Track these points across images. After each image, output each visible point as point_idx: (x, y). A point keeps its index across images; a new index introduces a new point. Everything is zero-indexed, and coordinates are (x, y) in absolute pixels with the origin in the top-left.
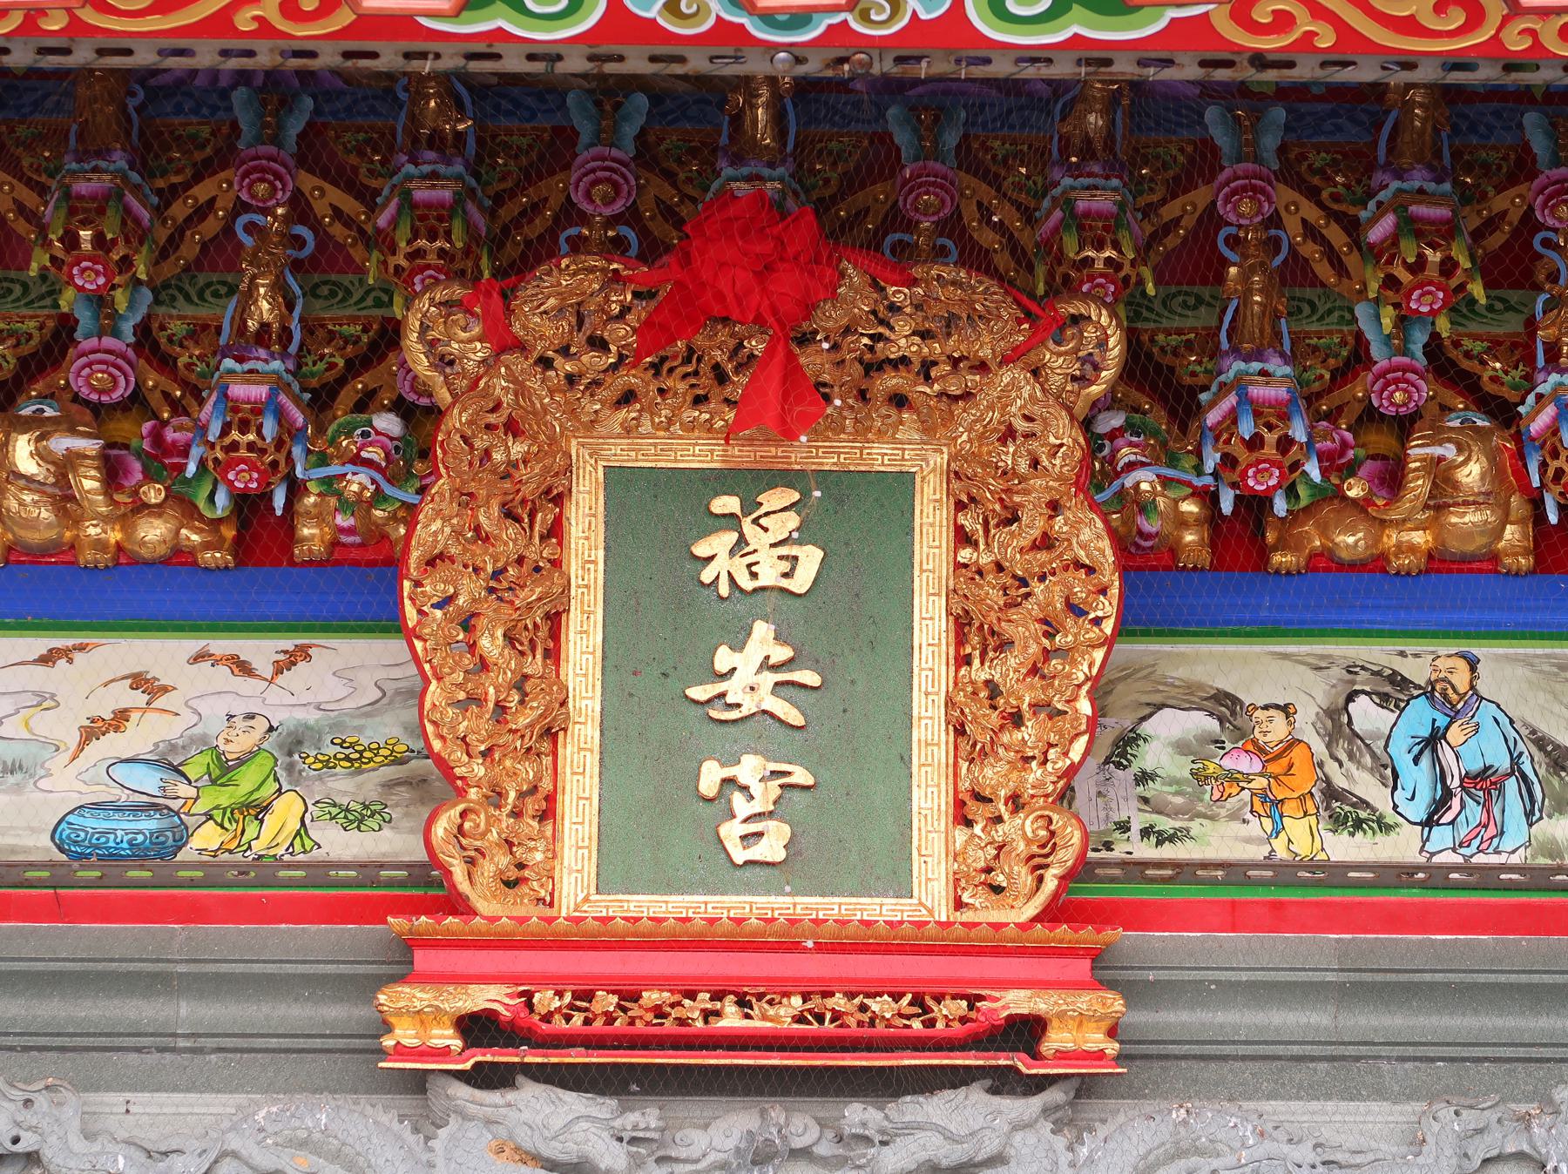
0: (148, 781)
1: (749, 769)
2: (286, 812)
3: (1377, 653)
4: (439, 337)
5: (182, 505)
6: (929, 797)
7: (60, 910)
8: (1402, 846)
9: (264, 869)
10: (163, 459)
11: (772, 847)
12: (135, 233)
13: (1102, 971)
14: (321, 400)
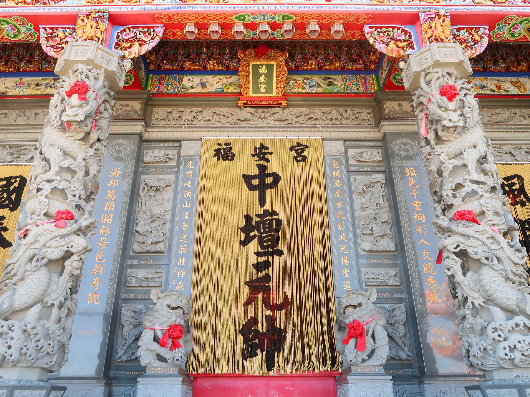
0: (221, 87)
1: (262, 86)
2: (231, 88)
3: (307, 76)
4: (240, 55)
5: (222, 66)
6: (274, 88)
7: (216, 96)
8: (307, 91)
9: (230, 93)
10: (221, 63)
11: (264, 91)
12: (218, 46)
13: (286, 99)
14: (232, 58)
